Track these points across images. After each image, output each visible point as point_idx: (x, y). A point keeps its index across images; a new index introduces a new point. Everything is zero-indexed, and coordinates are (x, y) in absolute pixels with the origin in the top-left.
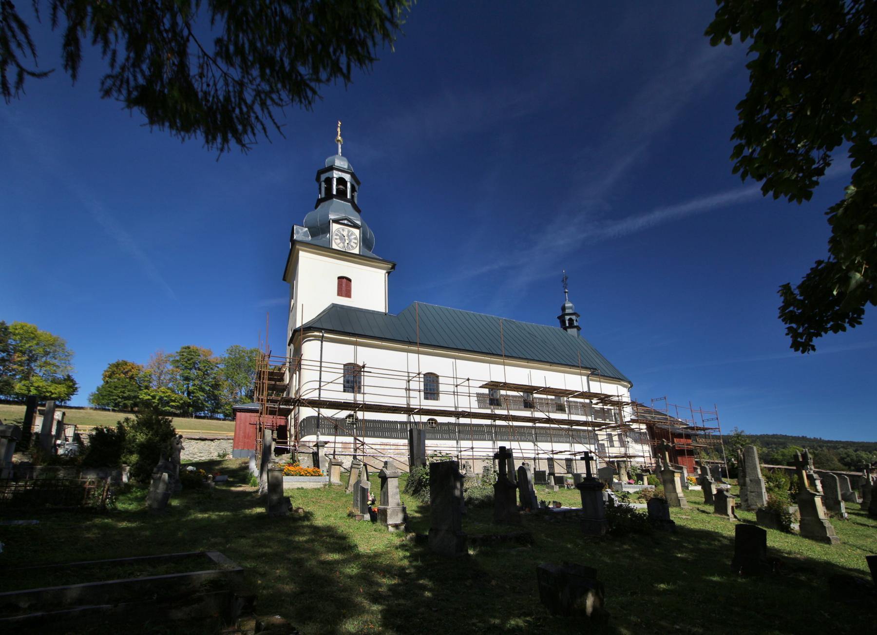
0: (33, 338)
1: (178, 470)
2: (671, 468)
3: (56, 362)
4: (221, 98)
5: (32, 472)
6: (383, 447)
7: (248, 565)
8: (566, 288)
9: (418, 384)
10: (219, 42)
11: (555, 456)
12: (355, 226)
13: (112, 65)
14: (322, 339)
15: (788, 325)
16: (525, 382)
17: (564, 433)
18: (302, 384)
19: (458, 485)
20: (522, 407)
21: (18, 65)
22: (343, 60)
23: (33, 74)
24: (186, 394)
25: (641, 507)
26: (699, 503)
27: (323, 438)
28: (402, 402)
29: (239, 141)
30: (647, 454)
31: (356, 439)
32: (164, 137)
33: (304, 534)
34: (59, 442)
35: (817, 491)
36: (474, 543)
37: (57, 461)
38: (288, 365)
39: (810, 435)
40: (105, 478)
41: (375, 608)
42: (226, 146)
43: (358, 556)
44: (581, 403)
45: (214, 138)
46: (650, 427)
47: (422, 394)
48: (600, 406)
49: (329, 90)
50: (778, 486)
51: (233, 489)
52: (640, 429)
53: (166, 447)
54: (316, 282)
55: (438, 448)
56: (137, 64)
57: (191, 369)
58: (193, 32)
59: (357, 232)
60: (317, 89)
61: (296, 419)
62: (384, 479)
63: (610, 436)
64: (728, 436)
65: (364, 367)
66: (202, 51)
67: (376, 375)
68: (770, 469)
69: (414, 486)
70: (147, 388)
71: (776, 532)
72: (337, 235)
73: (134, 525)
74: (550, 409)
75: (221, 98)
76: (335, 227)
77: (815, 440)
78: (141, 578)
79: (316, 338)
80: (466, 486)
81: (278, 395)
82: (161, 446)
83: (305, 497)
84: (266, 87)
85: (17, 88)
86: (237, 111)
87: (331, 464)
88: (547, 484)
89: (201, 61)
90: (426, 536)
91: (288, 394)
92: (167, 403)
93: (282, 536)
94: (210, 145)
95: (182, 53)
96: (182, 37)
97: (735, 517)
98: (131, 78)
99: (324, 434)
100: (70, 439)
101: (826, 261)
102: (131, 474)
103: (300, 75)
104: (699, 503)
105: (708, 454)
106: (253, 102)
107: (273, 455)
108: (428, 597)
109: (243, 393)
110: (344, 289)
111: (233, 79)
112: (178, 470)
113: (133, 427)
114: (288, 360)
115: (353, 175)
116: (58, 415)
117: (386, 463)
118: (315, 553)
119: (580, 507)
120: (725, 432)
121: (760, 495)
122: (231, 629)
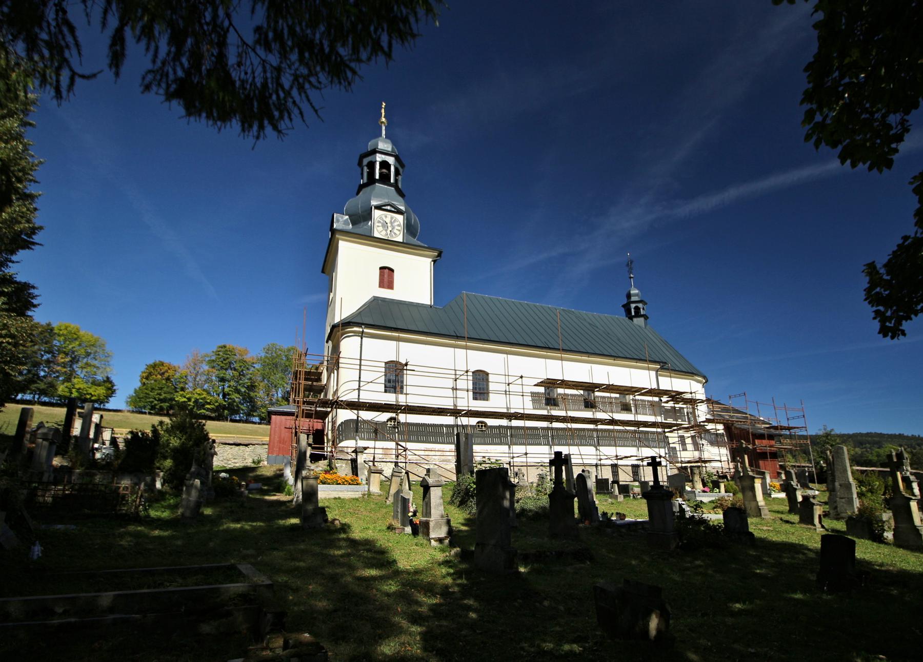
0: (76, 339)
1: (210, 476)
2: (751, 473)
3: (96, 363)
4: (259, 85)
5: (70, 477)
6: (427, 453)
7: (282, 578)
8: (631, 273)
9: (466, 383)
10: (258, 29)
11: (620, 462)
12: (399, 212)
13: (154, 62)
14: (362, 335)
15: (874, 308)
16: (586, 379)
17: (630, 435)
18: (340, 384)
19: (508, 495)
20: (583, 407)
21: (71, 70)
22: (385, 39)
23: (83, 77)
24: (221, 396)
25: (716, 517)
26: (782, 513)
27: (362, 444)
28: (448, 404)
29: (275, 128)
30: (724, 458)
31: (397, 444)
32: (201, 126)
33: (340, 548)
34: (96, 446)
35: (914, 495)
36: (526, 560)
37: (94, 463)
38: (325, 363)
39: (908, 433)
40: (138, 484)
41: (415, 629)
42: (262, 134)
43: (397, 573)
44: (648, 401)
45: (251, 126)
46: (728, 428)
47: (471, 394)
48: (671, 404)
49: (370, 70)
50: (871, 491)
51: (267, 498)
52: (717, 430)
53: (199, 453)
54: (356, 272)
55: (486, 453)
56: (177, 57)
57: (226, 369)
58: (234, 23)
59: (400, 218)
60: (357, 69)
61: (334, 423)
62: (426, 488)
63: (682, 438)
64: (816, 436)
65: (406, 365)
66: (242, 39)
67: (421, 373)
68: (862, 472)
69: (460, 497)
70: (183, 389)
71: (868, 542)
72: (379, 222)
73: (166, 534)
74: (614, 409)
75: (259, 85)
76: (377, 214)
77: (913, 437)
78: (171, 589)
79: (356, 334)
80: (518, 495)
81: (315, 396)
82: (198, 449)
83: (342, 507)
84: (304, 71)
85: (69, 91)
86: (274, 97)
87: (371, 472)
88: (611, 494)
89: (240, 50)
90: (473, 552)
91: (326, 395)
92: (202, 406)
93: (317, 549)
94: (247, 133)
95: (222, 44)
96: (222, 29)
97: (823, 527)
98: (171, 71)
99: (363, 439)
100: (108, 443)
101: (913, 235)
102: (164, 480)
103: (340, 56)
104: (782, 513)
105: (794, 456)
106: (291, 87)
107: (308, 462)
108: (472, 619)
109: (280, 395)
110: (386, 280)
111: (271, 65)
112: (210, 476)
113: (167, 431)
114: (326, 358)
115: (397, 158)
116: (96, 418)
117: (428, 470)
118: (352, 568)
119: (646, 519)
120: (812, 431)
121: (850, 501)
122: (259, 646)
